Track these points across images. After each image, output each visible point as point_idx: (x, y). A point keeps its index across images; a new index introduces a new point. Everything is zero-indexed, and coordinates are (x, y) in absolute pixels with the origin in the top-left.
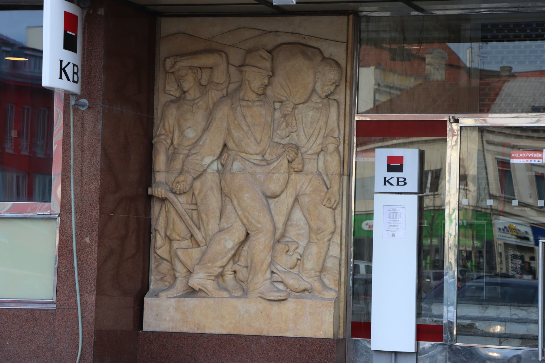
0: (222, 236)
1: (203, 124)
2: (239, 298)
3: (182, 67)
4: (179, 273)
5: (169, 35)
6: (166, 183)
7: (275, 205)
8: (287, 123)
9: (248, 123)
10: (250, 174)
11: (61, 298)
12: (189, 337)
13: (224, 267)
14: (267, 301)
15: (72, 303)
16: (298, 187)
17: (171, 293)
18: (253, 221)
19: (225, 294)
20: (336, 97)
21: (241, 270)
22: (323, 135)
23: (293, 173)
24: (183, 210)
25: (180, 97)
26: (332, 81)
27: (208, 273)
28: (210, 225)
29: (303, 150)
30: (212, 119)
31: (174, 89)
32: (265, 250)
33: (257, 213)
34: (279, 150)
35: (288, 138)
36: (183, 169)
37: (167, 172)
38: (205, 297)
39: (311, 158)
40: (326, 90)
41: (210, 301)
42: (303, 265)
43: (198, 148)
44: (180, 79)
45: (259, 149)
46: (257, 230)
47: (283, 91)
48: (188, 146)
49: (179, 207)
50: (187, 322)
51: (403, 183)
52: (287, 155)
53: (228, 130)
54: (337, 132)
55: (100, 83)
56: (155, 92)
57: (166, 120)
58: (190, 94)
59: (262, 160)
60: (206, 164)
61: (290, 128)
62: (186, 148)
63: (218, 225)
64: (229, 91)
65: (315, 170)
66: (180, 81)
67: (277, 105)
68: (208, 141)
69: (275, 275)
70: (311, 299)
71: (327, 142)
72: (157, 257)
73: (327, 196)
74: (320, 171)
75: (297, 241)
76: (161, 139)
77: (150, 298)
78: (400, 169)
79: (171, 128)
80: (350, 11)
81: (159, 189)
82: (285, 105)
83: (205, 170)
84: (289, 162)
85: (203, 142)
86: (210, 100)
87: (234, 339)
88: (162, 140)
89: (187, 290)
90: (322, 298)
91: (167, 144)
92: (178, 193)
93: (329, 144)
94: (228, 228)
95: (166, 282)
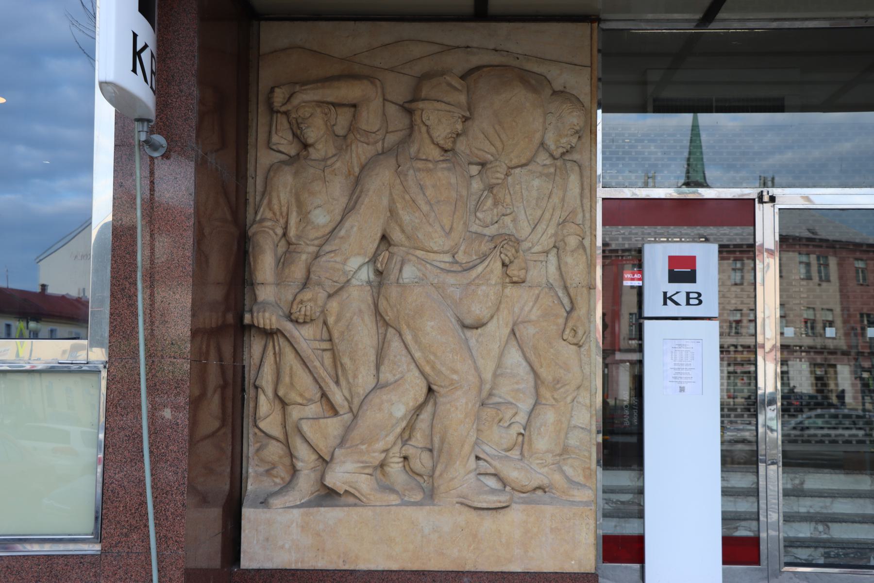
0: (384, 397)
1: (344, 201)
2: (420, 506)
4: (302, 461)
5: (275, 51)
6: (276, 303)
7: (477, 341)
8: (495, 198)
9: (429, 198)
10: (435, 287)
11: (112, 531)
12: (328, 576)
13: (386, 451)
14: (472, 510)
15: (136, 542)
16: (516, 310)
17: (291, 499)
18: (443, 369)
19: (393, 499)
20: (576, 156)
21: (418, 455)
22: (557, 221)
23: (508, 284)
24: (310, 350)
25: (298, 154)
26: (575, 128)
27: (362, 462)
28: (360, 376)
29: (526, 245)
30: (361, 191)
32: (467, 420)
33: (451, 355)
34: (482, 245)
36: (308, 278)
37: (278, 285)
38: (355, 505)
39: (537, 259)
40: (564, 143)
41: (367, 513)
42: (531, 444)
44: (302, 123)
45: (448, 244)
46: (452, 384)
48: (317, 238)
49: (304, 347)
50: (324, 551)
51: (697, 302)
52: (501, 253)
53: (390, 211)
54: (580, 216)
55: (191, 104)
57: (274, 194)
58: (318, 150)
59: (452, 263)
60: (352, 269)
61: (500, 207)
62: (312, 243)
63: (372, 376)
64: (386, 145)
65: (544, 281)
66: (302, 126)
67: (474, 170)
68: (355, 229)
69: (481, 463)
70: (551, 504)
71: (565, 231)
72: (259, 433)
73: (570, 324)
74: (551, 281)
75: (514, 402)
76: (263, 227)
77: (252, 510)
78: (691, 277)
79: (283, 208)
80: (594, 17)
81: (267, 315)
82: (492, 168)
83: (348, 281)
84: (504, 265)
85: (346, 231)
86: (355, 161)
87: (413, 579)
88: (267, 229)
89: (317, 491)
90: (570, 501)
91: (275, 237)
92: (301, 320)
93: (569, 235)
94: (396, 382)
95: (276, 477)
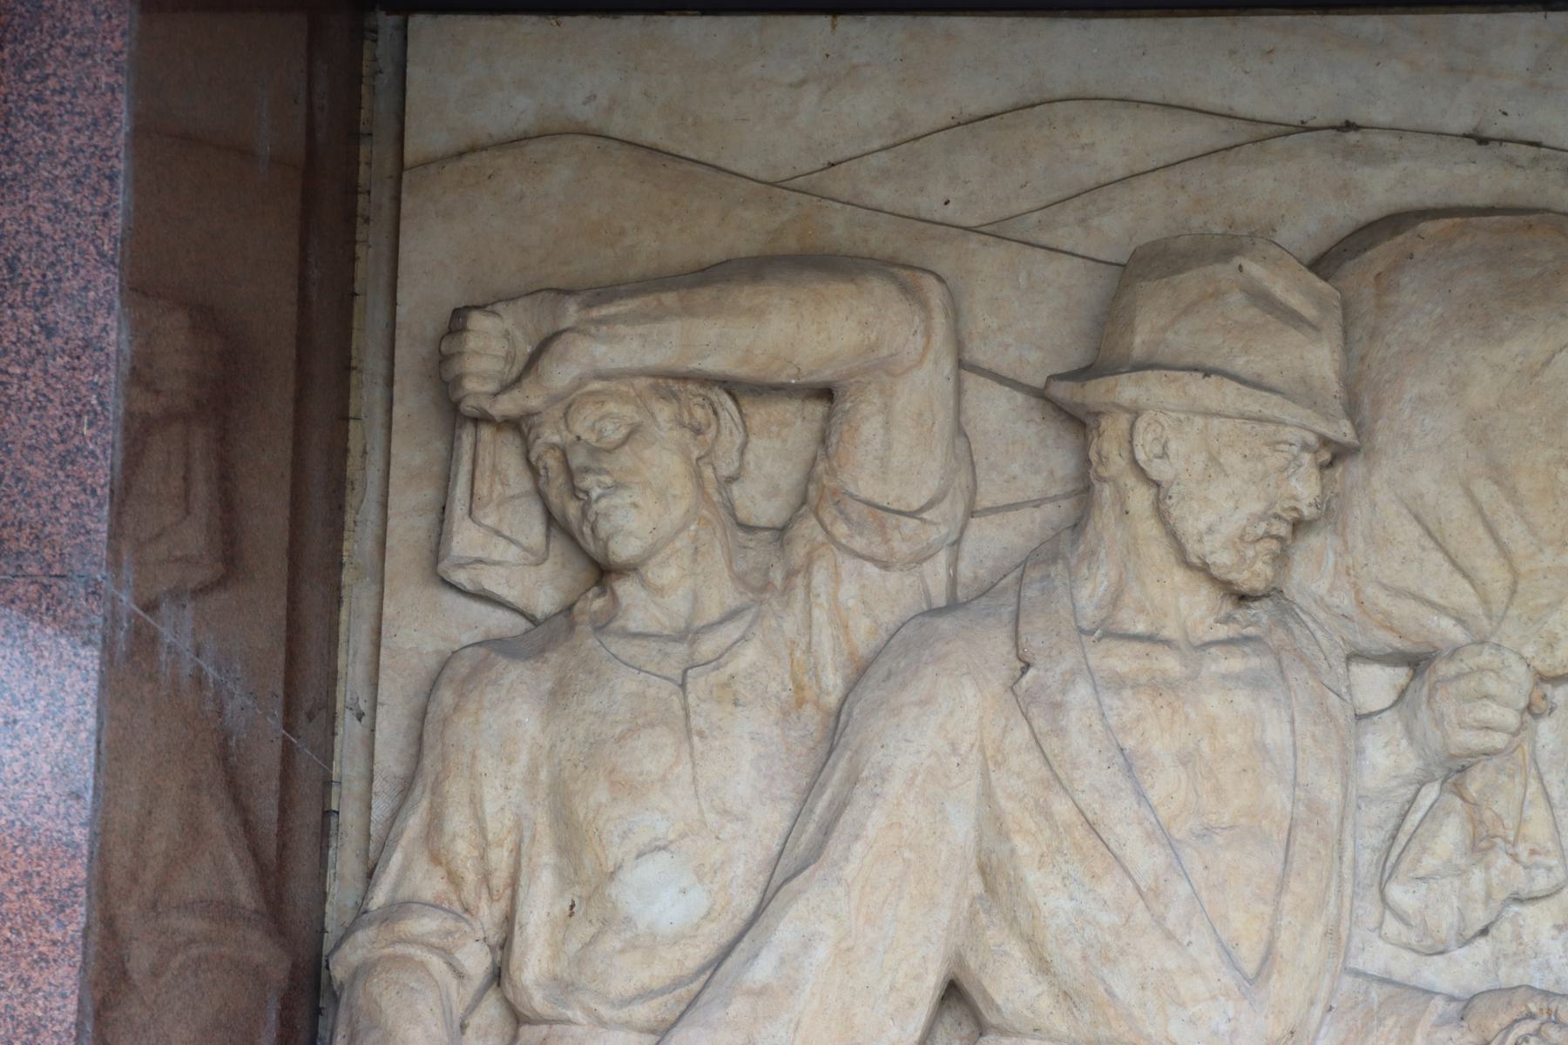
1: (771, 820)
3: (600, 376)
8: (1475, 818)
9: (1163, 813)
25: (568, 609)
30: (853, 780)
31: (514, 549)
35: (1482, 941)
43: (739, 1007)
44: (587, 470)
47: (1446, 566)
48: (645, 995)
53: (983, 870)
55: (94, 387)
56: (347, 577)
57: (456, 789)
58: (660, 591)
61: (1501, 861)
62: (623, 1014)
64: (965, 570)
66: (589, 481)
68: (822, 952)
76: (402, 941)
85: (782, 961)
86: (825, 639)
88: (417, 952)
91: (453, 983)
